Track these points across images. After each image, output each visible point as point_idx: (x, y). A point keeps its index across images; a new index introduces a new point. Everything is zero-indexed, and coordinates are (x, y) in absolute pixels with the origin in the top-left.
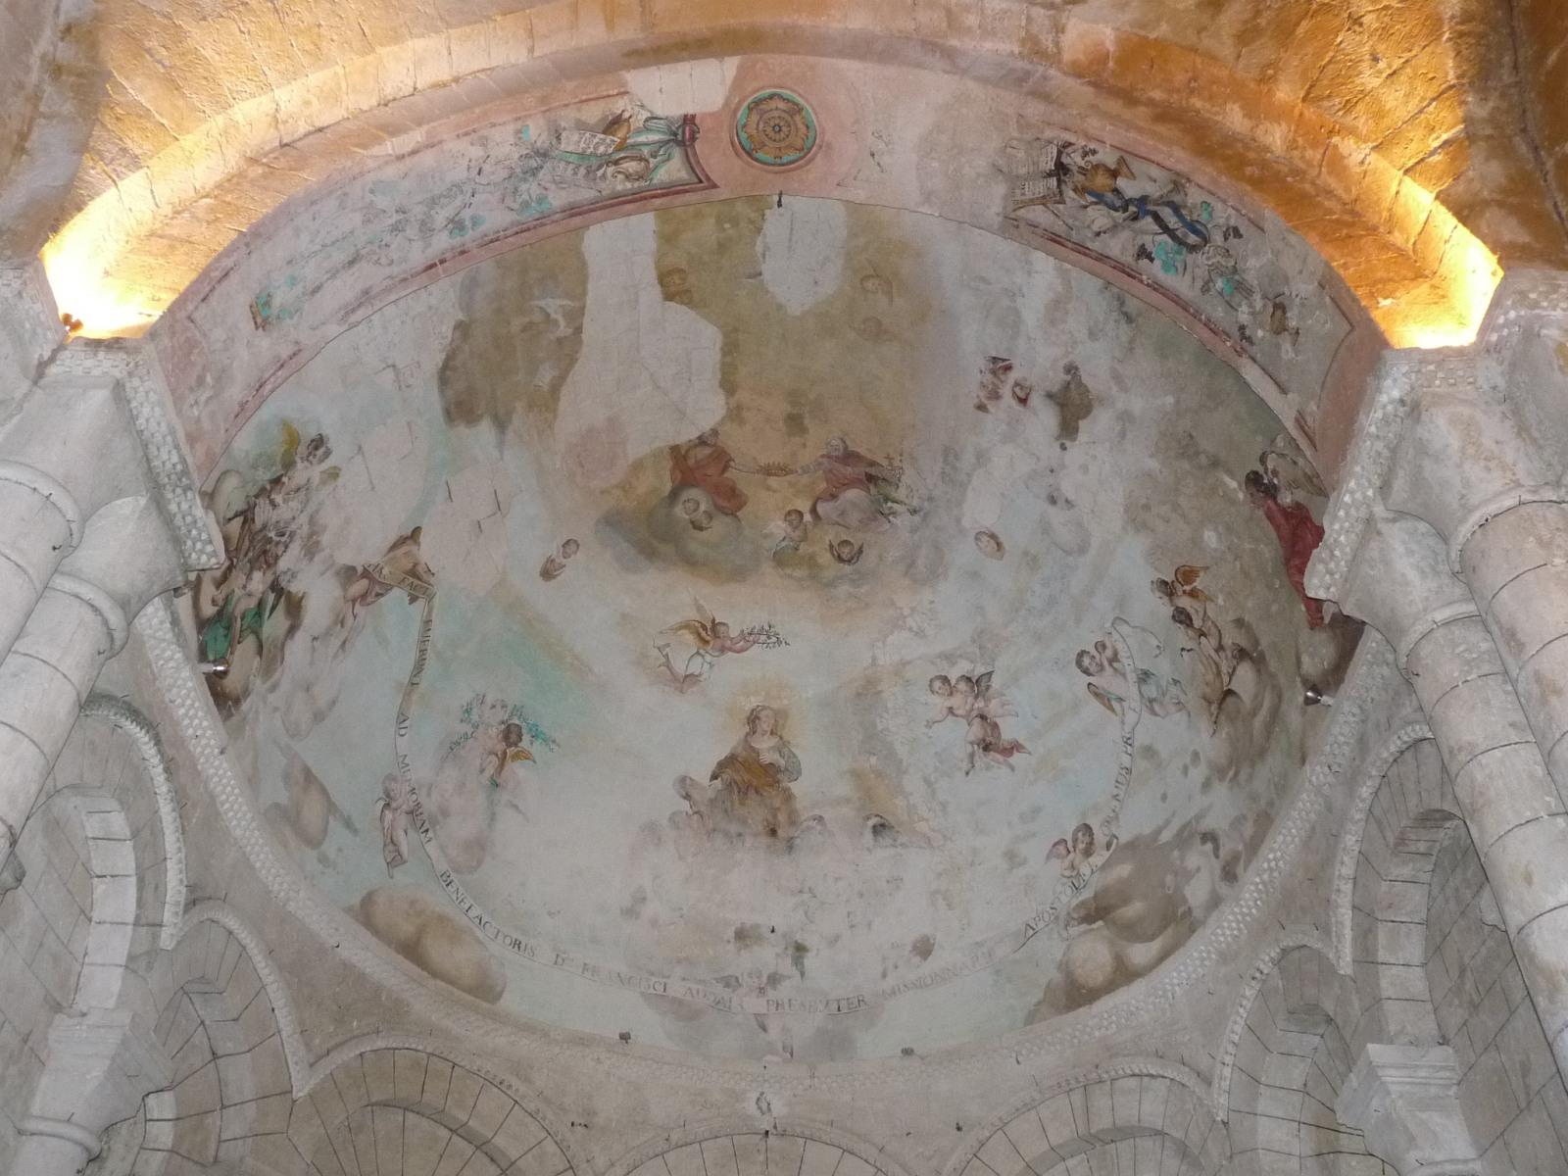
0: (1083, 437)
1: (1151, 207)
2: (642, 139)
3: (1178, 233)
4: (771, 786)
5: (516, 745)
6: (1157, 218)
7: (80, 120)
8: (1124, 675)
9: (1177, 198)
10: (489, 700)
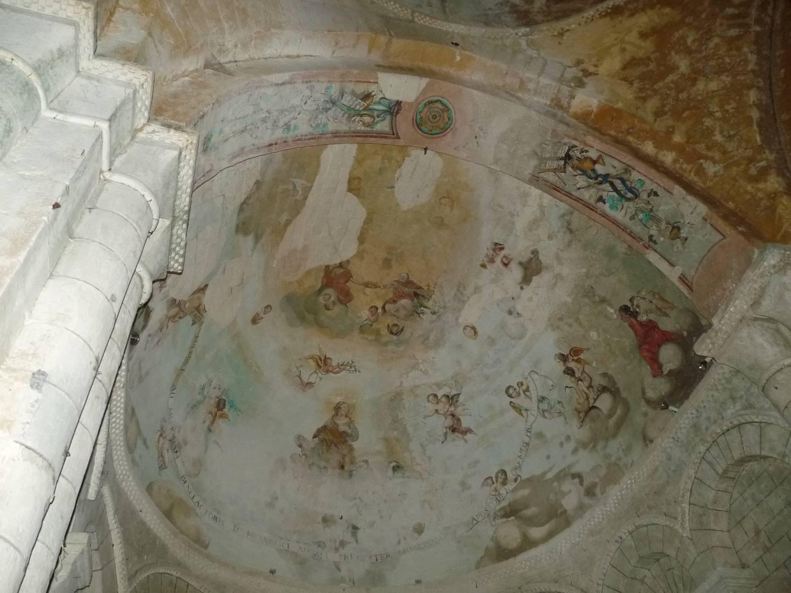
0: (533, 284)
1: (610, 179)
2: (376, 107)
3: (622, 192)
4: (343, 443)
5: (222, 411)
6: (612, 184)
7: (144, 14)
8: (531, 399)
9: (625, 177)
10: (213, 384)
